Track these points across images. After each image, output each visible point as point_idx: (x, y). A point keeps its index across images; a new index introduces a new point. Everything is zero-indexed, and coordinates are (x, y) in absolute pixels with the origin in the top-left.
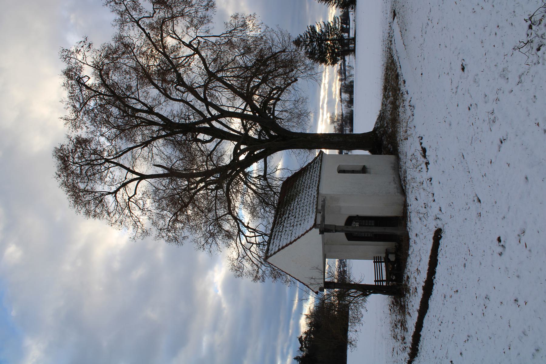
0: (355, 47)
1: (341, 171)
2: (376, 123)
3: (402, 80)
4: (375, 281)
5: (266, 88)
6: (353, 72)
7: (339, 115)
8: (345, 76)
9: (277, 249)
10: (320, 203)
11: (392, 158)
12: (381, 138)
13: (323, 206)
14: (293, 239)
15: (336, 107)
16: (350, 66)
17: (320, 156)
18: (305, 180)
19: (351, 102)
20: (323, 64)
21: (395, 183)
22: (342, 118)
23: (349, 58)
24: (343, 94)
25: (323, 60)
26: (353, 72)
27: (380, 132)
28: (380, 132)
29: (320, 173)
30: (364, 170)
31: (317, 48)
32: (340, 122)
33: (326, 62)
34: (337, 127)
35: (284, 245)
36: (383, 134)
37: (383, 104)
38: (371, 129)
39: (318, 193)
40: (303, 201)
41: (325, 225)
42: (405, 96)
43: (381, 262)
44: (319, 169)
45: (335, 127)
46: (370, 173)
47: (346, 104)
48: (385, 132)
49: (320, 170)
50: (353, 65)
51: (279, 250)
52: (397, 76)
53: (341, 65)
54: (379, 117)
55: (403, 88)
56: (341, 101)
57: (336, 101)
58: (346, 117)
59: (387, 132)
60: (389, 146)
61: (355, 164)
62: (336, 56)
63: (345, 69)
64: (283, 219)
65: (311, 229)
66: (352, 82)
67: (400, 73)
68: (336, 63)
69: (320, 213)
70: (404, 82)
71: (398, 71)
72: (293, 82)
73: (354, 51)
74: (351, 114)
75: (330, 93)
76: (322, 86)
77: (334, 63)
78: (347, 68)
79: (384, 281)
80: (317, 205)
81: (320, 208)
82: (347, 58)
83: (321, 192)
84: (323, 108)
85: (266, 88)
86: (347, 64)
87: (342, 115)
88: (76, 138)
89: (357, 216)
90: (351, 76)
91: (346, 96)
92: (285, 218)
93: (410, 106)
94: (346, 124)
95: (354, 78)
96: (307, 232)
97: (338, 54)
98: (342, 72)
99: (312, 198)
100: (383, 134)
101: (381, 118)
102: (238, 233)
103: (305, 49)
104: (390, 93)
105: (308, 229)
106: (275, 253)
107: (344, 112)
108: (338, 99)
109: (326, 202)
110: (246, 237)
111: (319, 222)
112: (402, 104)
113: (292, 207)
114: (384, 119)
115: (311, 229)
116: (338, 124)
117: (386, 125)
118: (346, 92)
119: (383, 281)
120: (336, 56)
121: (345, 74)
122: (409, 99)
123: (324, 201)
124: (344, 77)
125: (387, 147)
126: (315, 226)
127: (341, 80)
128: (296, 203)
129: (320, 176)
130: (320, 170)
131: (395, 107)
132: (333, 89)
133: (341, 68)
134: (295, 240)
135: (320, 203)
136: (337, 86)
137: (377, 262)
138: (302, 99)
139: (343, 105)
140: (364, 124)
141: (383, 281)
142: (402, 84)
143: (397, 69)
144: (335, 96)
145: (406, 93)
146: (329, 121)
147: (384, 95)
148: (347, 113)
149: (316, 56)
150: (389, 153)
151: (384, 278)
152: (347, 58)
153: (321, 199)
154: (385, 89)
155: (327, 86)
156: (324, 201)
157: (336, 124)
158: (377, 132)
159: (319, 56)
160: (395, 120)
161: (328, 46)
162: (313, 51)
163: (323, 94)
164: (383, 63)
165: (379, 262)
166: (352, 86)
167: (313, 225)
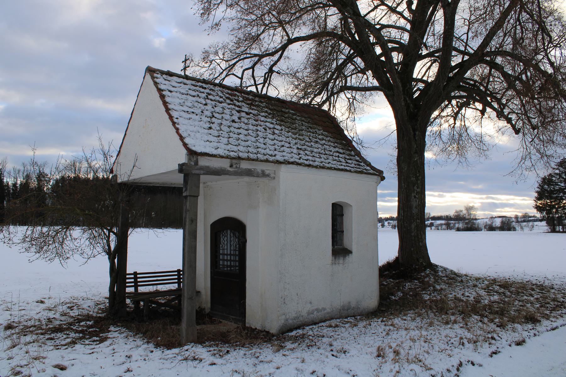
0: (559, 232)
1: (338, 210)
2: (445, 269)
3: (525, 334)
4: (135, 274)
5: (497, 84)
6: (526, 230)
7: (475, 215)
8: (522, 222)
9: (162, 87)
10: (259, 167)
11: (372, 300)
12: (417, 279)
13: (249, 173)
14: (174, 114)
15: (487, 212)
16: (533, 227)
17: (371, 171)
18: (323, 145)
19: (491, 228)
20: (536, 195)
21: (309, 313)
22: (473, 219)
23: (543, 226)
24: (500, 219)
25: (541, 195)
26: (526, 230)
27: (428, 276)
28: (428, 276)
29: (330, 168)
30: (340, 250)
31: (557, 188)
32: (467, 217)
33: (538, 199)
34: (462, 214)
35: (167, 99)
36: (422, 282)
37: (477, 279)
38: (435, 258)
39: (278, 162)
40: (272, 137)
41: (199, 175)
42: (487, 349)
43: (179, 283)
44: (343, 167)
45: (461, 211)
46: (333, 264)
47: (489, 223)
48: (425, 286)
49: (335, 169)
50: (535, 230)
51: (160, 90)
52: (532, 320)
53: (534, 216)
54: (455, 274)
55: (506, 337)
56: (492, 218)
57: (493, 212)
58: (474, 224)
59: (424, 289)
60: (400, 294)
61: (354, 236)
62: (547, 210)
63: (529, 221)
64: (240, 104)
65: (185, 145)
66: (514, 229)
67: (539, 328)
68: (538, 210)
69: (231, 166)
70: (519, 343)
71: (545, 322)
72: (513, 127)
73: (554, 231)
74: (477, 229)
75: (503, 205)
76: (512, 197)
77: (538, 208)
78: (531, 223)
79: (136, 289)
80: (248, 159)
81: (244, 165)
82: (544, 223)
83: (283, 167)
84: (487, 198)
85: (497, 84)
86: (536, 223)
87: (476, 219)
88: (540, 321)
89: (246, 241)
90: (522, 228)
91: (498, 222)
92: (239, 106)
93: (461, 364)
94: (466, 223)
95: (520, 232)
96: (182, 138)
97: (549, 212)
98: (526, 219)
99: (270, 153)
100: (422, 282)
101: (453, 278)
102: (255, 55)
103: (556, 174)
104: (496, 297)
105: (187, 141)
106: (156, 84)
107: (478, 221)
108: (495, 214)
109: (265, 180)
110: (253, 68)
111: (203, 162)
112: (469, 335)
113: (263, 119)
114: (450, 284)
115: (185, 145)
116: (465, 214)
117: (438, 287)
118: (502, 222)
119: (136, 286)
120: (547, 210)
121: (524, 221)
122: (476, 358)
123: (264, 175)
124: (519, 220)
125: (399, 290)
126: (192, 153)
127: (517, 217)
128: (272, 126)
129: (323, 168)
130: (335, 169)
131: (470, 310)
132: (507, 209)
133: (531, 217)
134: (171, 117)
135: (259, 167)
136: (510, 213)
137: (179, 275)
138: (485, 148)
139: (487, 220)
140: (441, 248)
141: (136, 286)
142: (517, 337)
143: (547, 317)
144: (499, 212)
145: (494, 348)
146: (471, 205)
147: (494, 281)
148: (478, 224)
149: (546, 186)
150: (385, 295)
151: (141, 289)
152: (544, 223)
153: (268, 168)
154: (506, 285)
155: (511, 202)
156: (264, 175)
157: (465, 212)
158: (428, 271)
159: (547, 190)
160: (441, 309)
161: (560, 200)
162: (553, 182)
163: (503, 198)
164: (550, 277)
165: (179, 279)
166: (509, 229)
167: (193, 149)
